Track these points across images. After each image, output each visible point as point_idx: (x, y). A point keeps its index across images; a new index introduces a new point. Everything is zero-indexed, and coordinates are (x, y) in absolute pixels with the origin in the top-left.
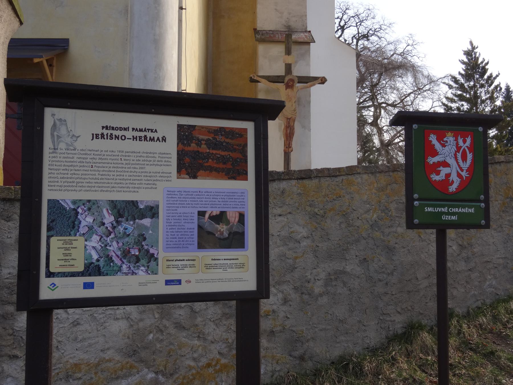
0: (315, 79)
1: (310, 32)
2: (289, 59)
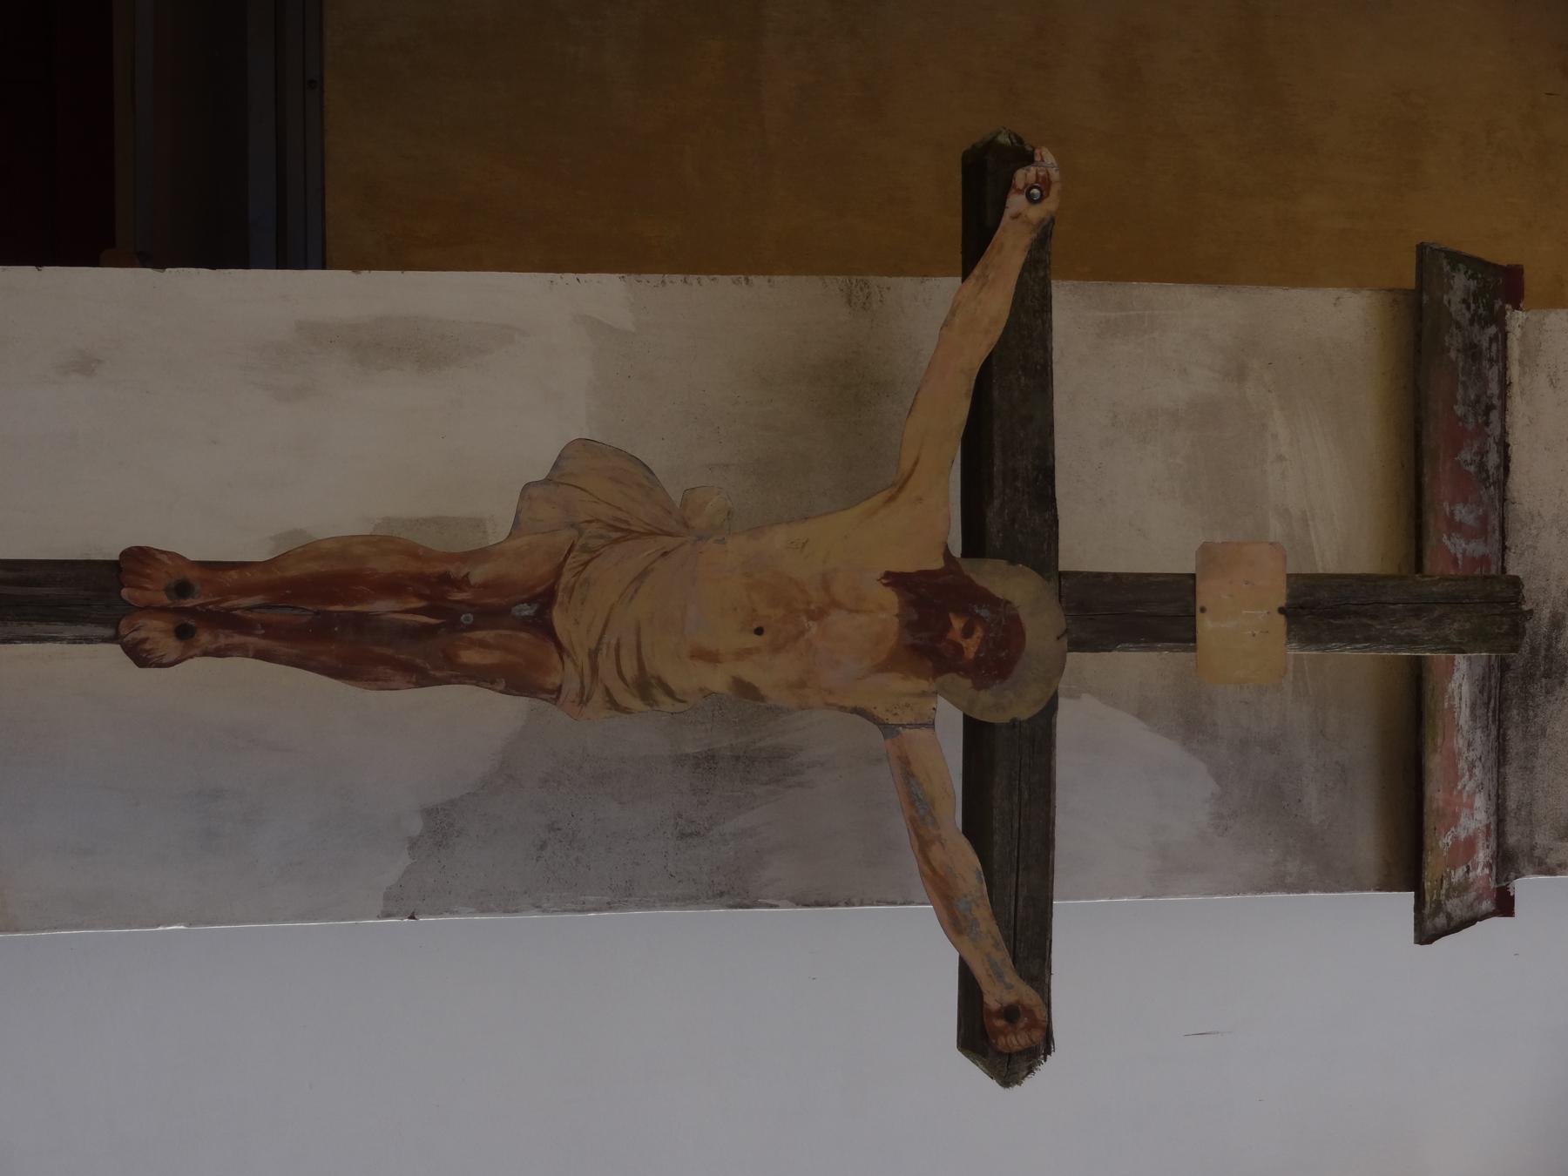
0: (1029, 945)
1: (1505, 906)
2: (1240, 623)
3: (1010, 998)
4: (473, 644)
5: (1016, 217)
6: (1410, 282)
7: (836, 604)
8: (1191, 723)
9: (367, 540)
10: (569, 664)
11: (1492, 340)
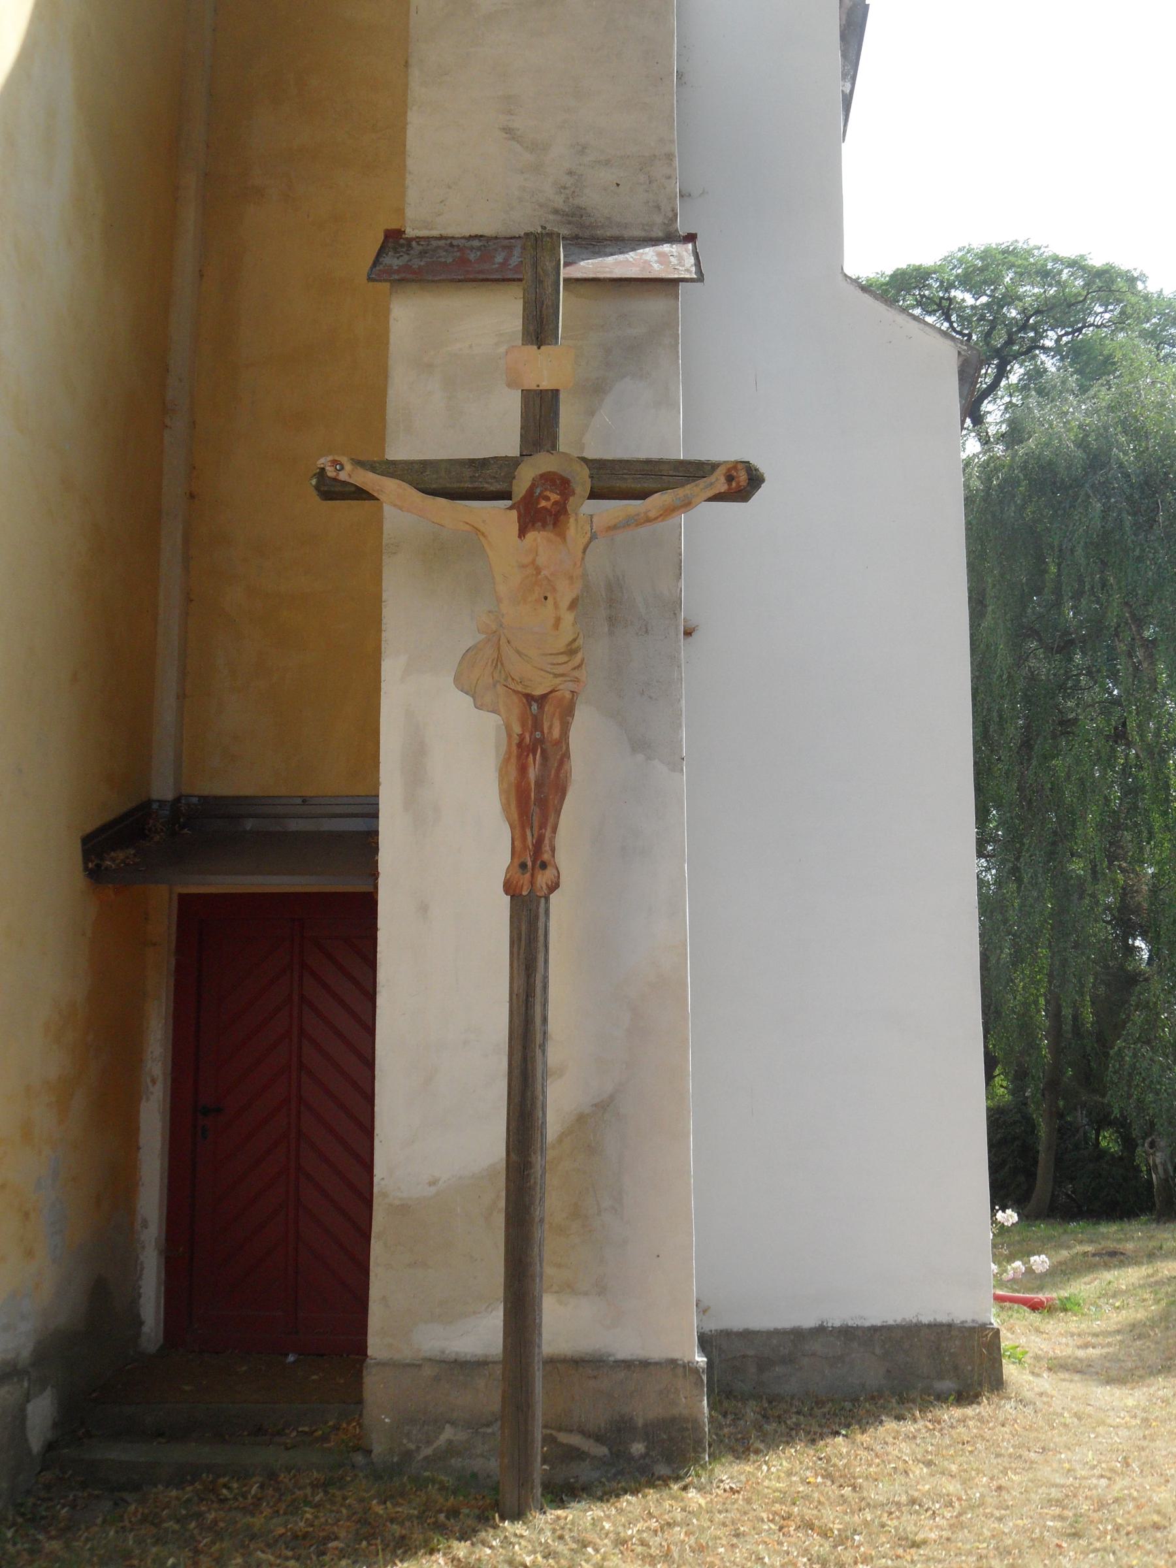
0: (693, 471)
2: (546, 368)
3: (723, 479)
4: (550, 732)
5: (350, 476)
6: (387, 285)
7: (533, 562)
8: (596, 390)
9: (501, 782)
10: (561, 687)
11: (418, 244)
